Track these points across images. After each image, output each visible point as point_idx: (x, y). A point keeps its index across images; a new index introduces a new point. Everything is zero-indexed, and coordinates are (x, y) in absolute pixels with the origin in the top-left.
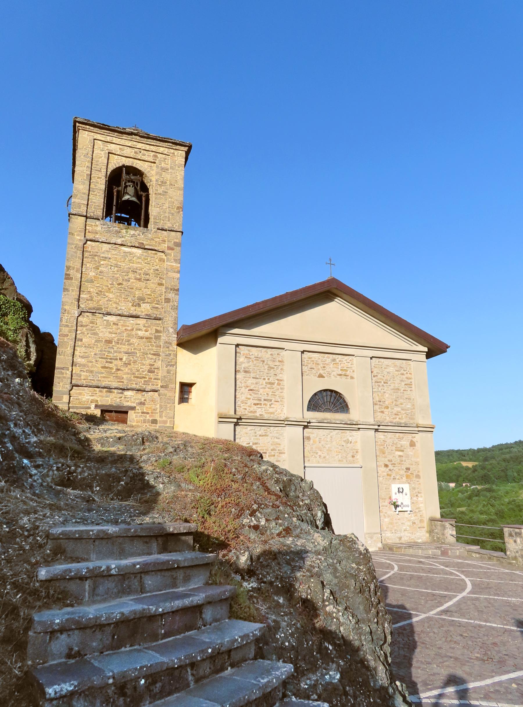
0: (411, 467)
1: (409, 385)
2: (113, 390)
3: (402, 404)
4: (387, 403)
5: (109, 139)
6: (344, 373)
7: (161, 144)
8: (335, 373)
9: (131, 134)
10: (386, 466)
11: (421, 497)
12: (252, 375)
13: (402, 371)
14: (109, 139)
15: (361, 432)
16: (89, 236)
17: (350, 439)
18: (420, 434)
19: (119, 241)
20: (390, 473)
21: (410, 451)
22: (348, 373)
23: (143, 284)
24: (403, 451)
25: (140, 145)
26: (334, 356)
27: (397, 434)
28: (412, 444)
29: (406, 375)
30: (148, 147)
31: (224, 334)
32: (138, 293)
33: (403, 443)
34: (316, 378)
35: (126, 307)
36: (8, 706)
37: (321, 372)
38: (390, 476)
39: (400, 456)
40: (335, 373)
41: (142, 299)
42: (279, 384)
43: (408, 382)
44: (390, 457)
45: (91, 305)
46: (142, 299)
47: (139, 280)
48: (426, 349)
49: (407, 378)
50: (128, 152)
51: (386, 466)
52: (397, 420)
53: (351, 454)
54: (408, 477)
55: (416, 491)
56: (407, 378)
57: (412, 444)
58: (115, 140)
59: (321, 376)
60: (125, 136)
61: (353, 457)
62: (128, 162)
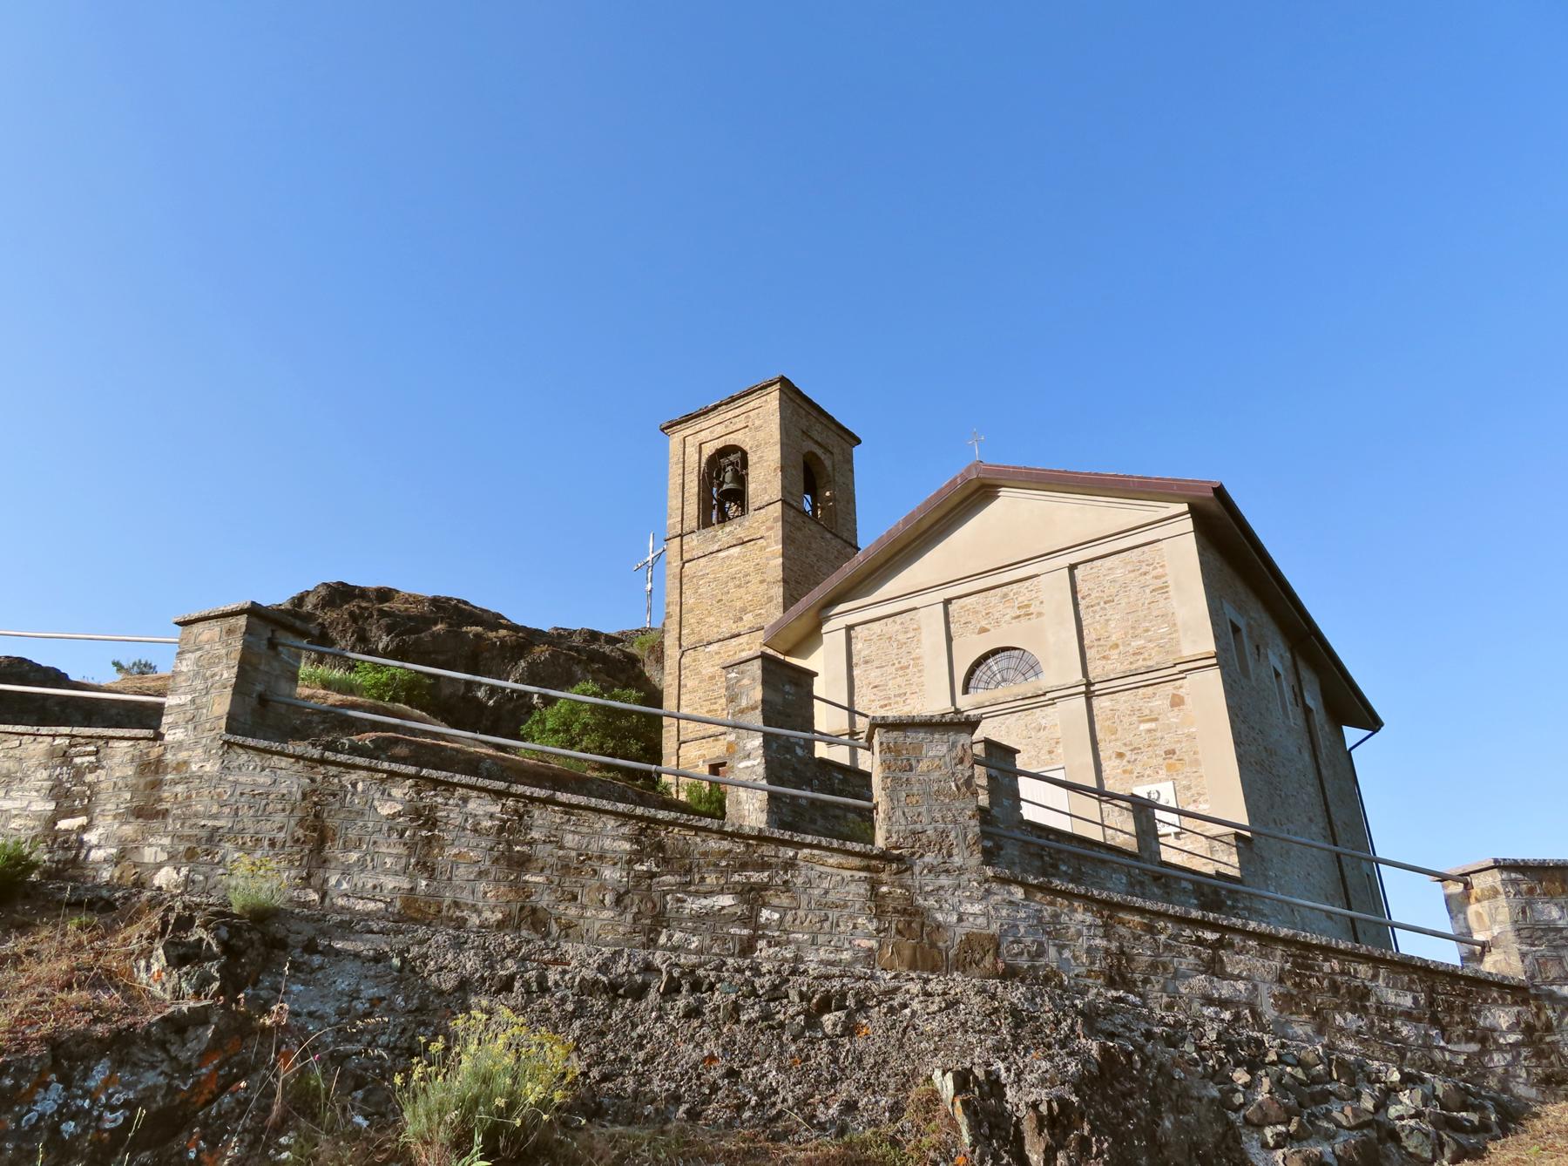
0: (1177, 747)
1: (1163, 589)
2: (585, 757)
3: (1147, 631)
4: (1114, 638)
5: (697, 428)
6: (1023, 611)
7: (747, 399)
8: (1007, 618)
9: (716, 407)
10: (1120, 755)
11: (1206, 801)
12: (876, 663)
13: (1145, 568)
14: (697, 428)
15: (1060, 704)
16: (686, 556)
17: (1043, 722)
18: (1191, 677)
19: (716, 548)
20: (1129, 767)
21: (1173, 717)
22: (1032, 610)
23: (743, 590)
24: (1156, 720)
25: (730, 415)
26: (1004, 589)
27: (1141, 691)
28: (1177, 702)
29: (1154, 573)
30: (737, 412)
31: (828, 619)
32: (739, 604)
33: (1156, 703)
34: (975, 637)
35: (728, 627)
36: (122, 1162)
37: (983, 623)
38: (1131, 772)
39: (1149, 731)
40: (1007, 618)
41: (744, 610)
42: (916, 665)
43: (1159, 583)
44: (1129, 737)
45: (693, 639)
46: (744, 610)
47: (739, 586)
48: (1185, 507)
49: (1156, 578)
50: (720, 430)
51: (1120, 755)
52: (1141, 663)
53: (1047, 749)
54: (1170, 767)
55: (1193, 791)
56: (1156, 578)
57: (1177, 702)
58: (705, 425)
59: (983, 630)
60: (711, 415)
61: (1050, 752)
62: (719, 444)
